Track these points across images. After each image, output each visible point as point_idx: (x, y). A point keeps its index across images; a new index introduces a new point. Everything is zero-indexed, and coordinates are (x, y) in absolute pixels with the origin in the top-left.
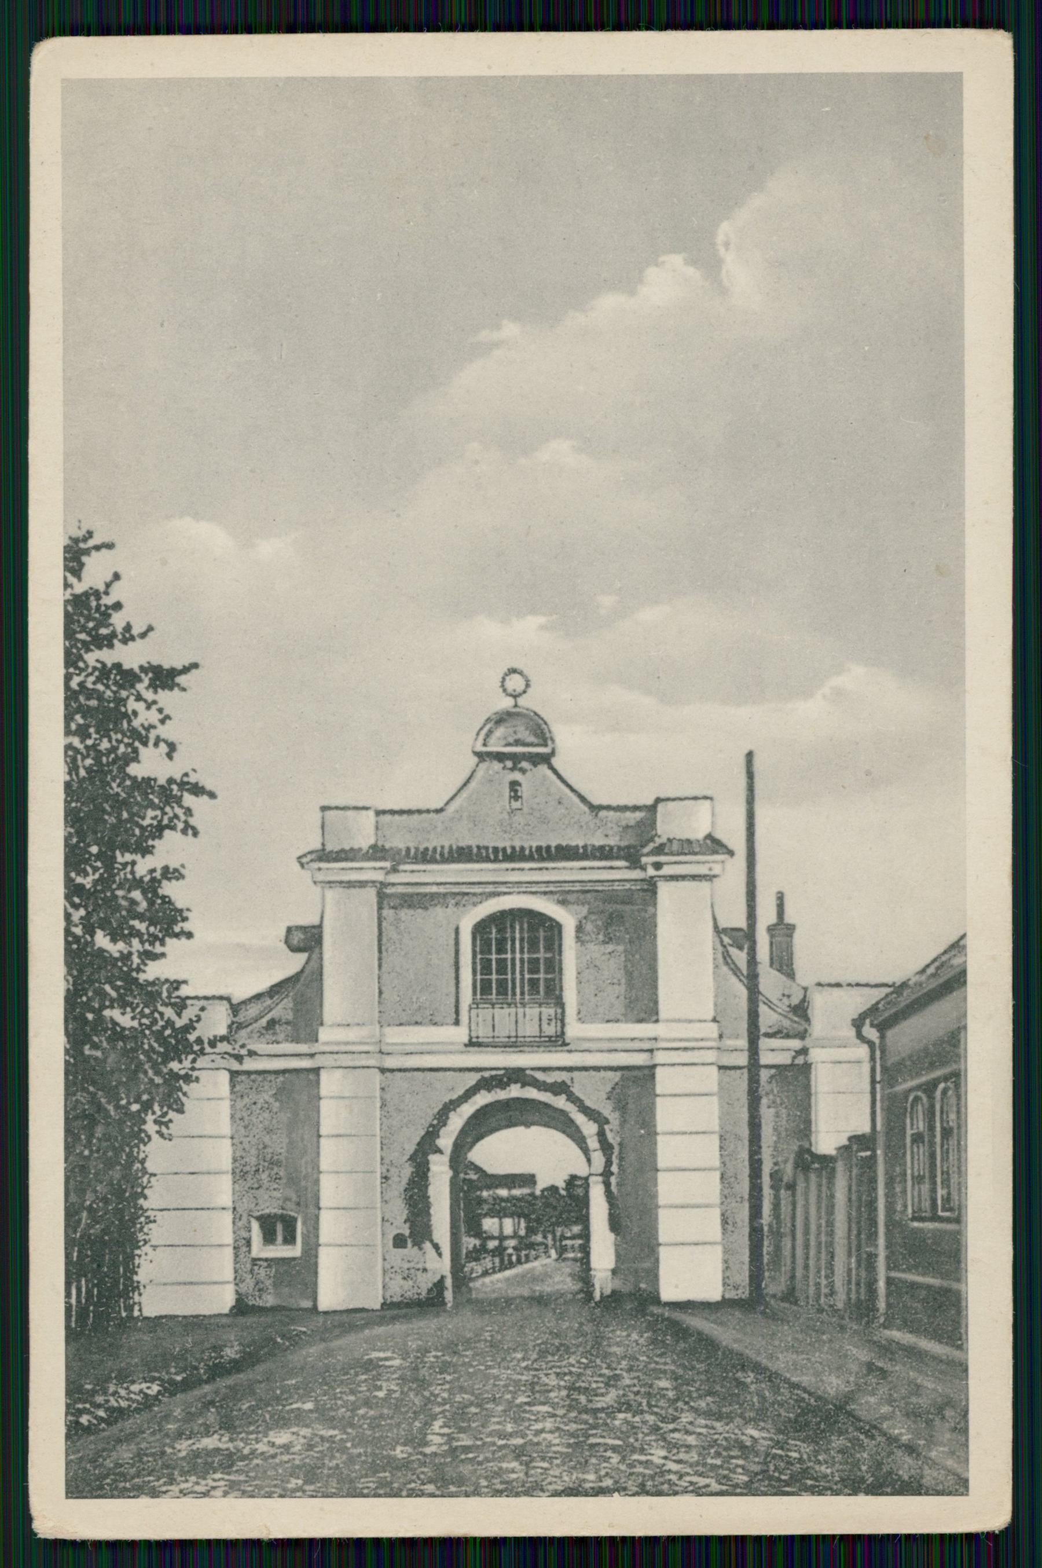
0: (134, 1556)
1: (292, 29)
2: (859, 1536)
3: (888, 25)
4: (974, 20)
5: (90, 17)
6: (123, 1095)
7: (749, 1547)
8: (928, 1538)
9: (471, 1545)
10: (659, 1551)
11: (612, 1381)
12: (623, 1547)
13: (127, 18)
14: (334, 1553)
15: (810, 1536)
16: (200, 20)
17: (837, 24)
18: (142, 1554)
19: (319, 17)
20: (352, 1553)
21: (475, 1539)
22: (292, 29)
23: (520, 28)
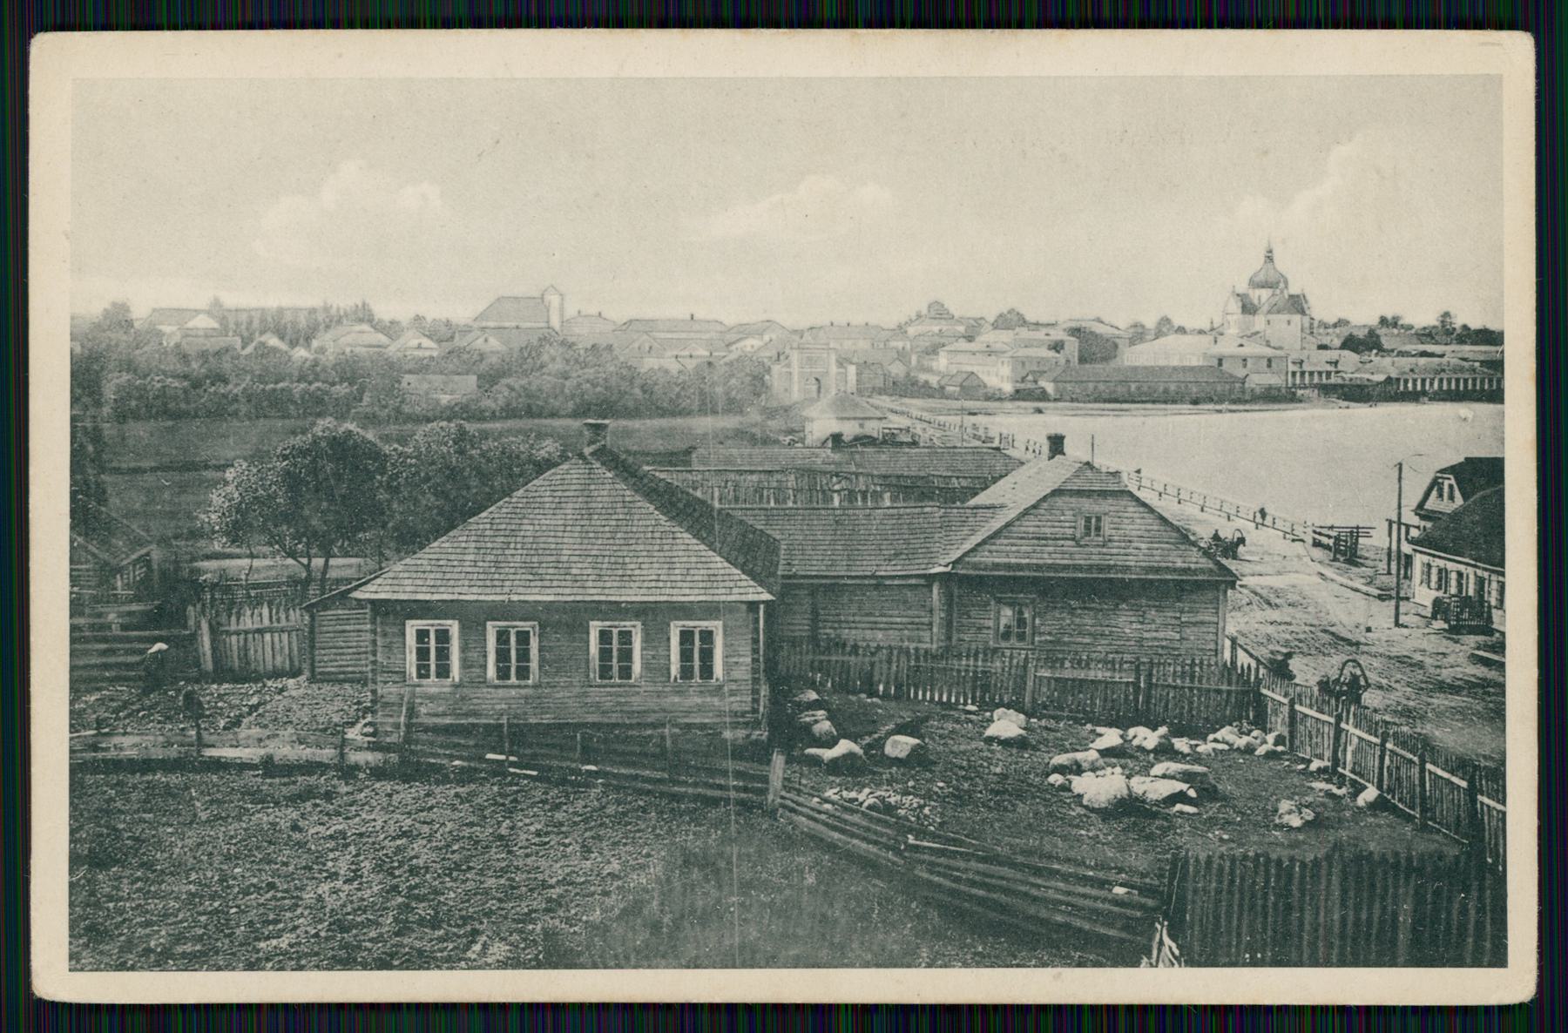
0: (506, 1020)
1: (664, 24)
2: (1231, 1006)
3: (1260, 25)
4: (1326, 18)
5: (462, 11)
6: (439, 518)
7: (1121, 1016)
8: (1300, 1010)
9: (843, 1010)
10: (1031, 1019)
11: (695, 510)
12: (995, 1015)
13: (498, 10)
14: (706, 1016)
15: (1181, 1006)
16: (276, 17)
17: (1208, 24)
18: (514, 1017)
19: (266, 17)
20: (724, 1018)
21: (847, 1005)
22: (663, 24)
23: (892, 25)
